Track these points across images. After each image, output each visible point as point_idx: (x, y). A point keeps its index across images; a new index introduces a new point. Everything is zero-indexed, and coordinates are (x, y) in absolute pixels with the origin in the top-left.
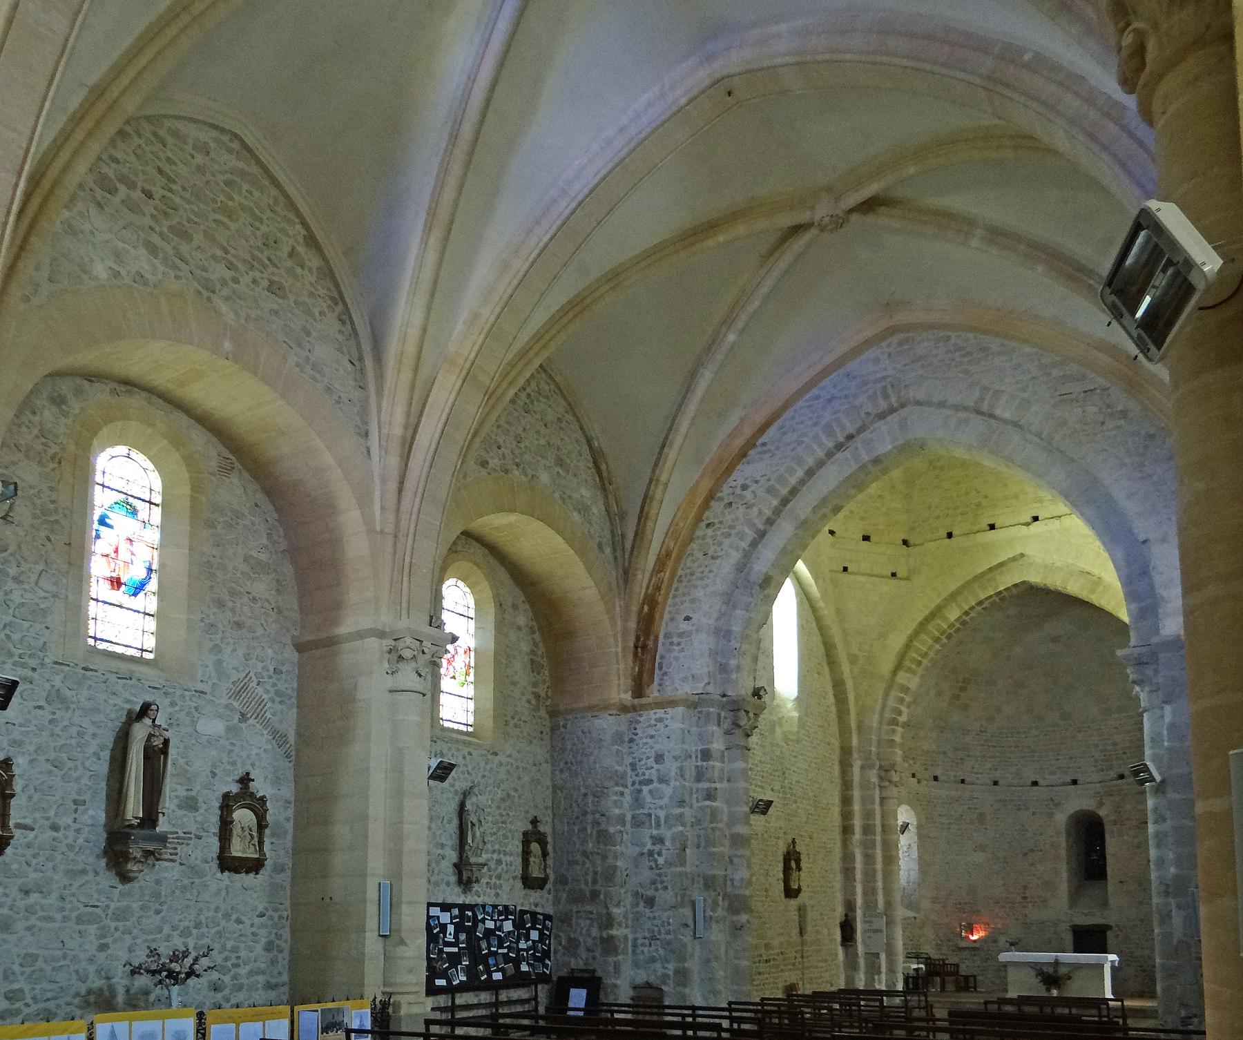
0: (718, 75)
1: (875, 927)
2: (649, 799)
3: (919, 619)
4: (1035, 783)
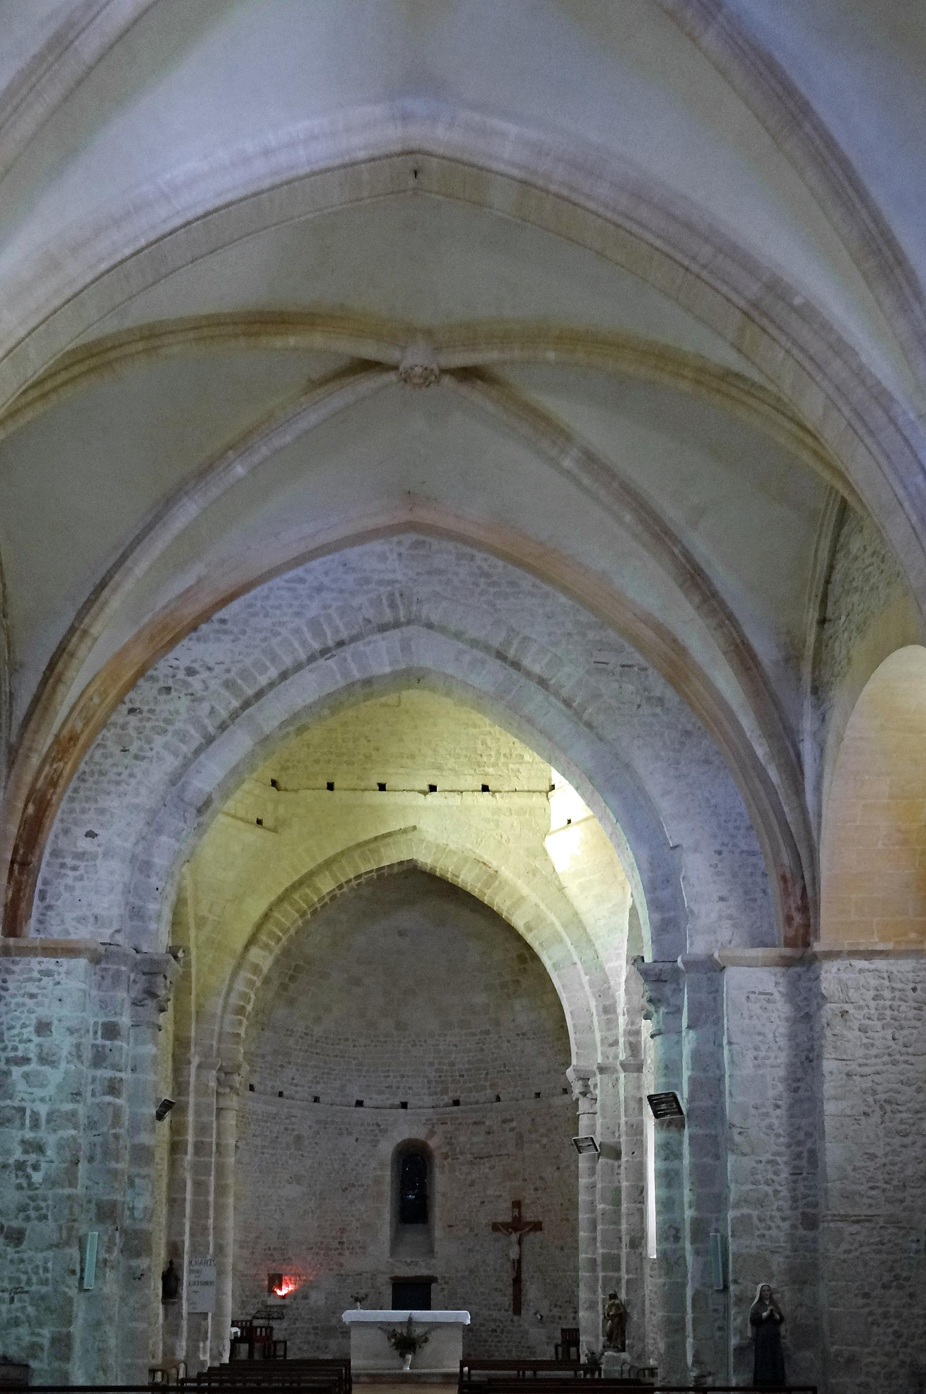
0: (414, 145)
1: (203, 1278)
2: (21, 1086)
3: (287, 884)
4: (359, 1104)
